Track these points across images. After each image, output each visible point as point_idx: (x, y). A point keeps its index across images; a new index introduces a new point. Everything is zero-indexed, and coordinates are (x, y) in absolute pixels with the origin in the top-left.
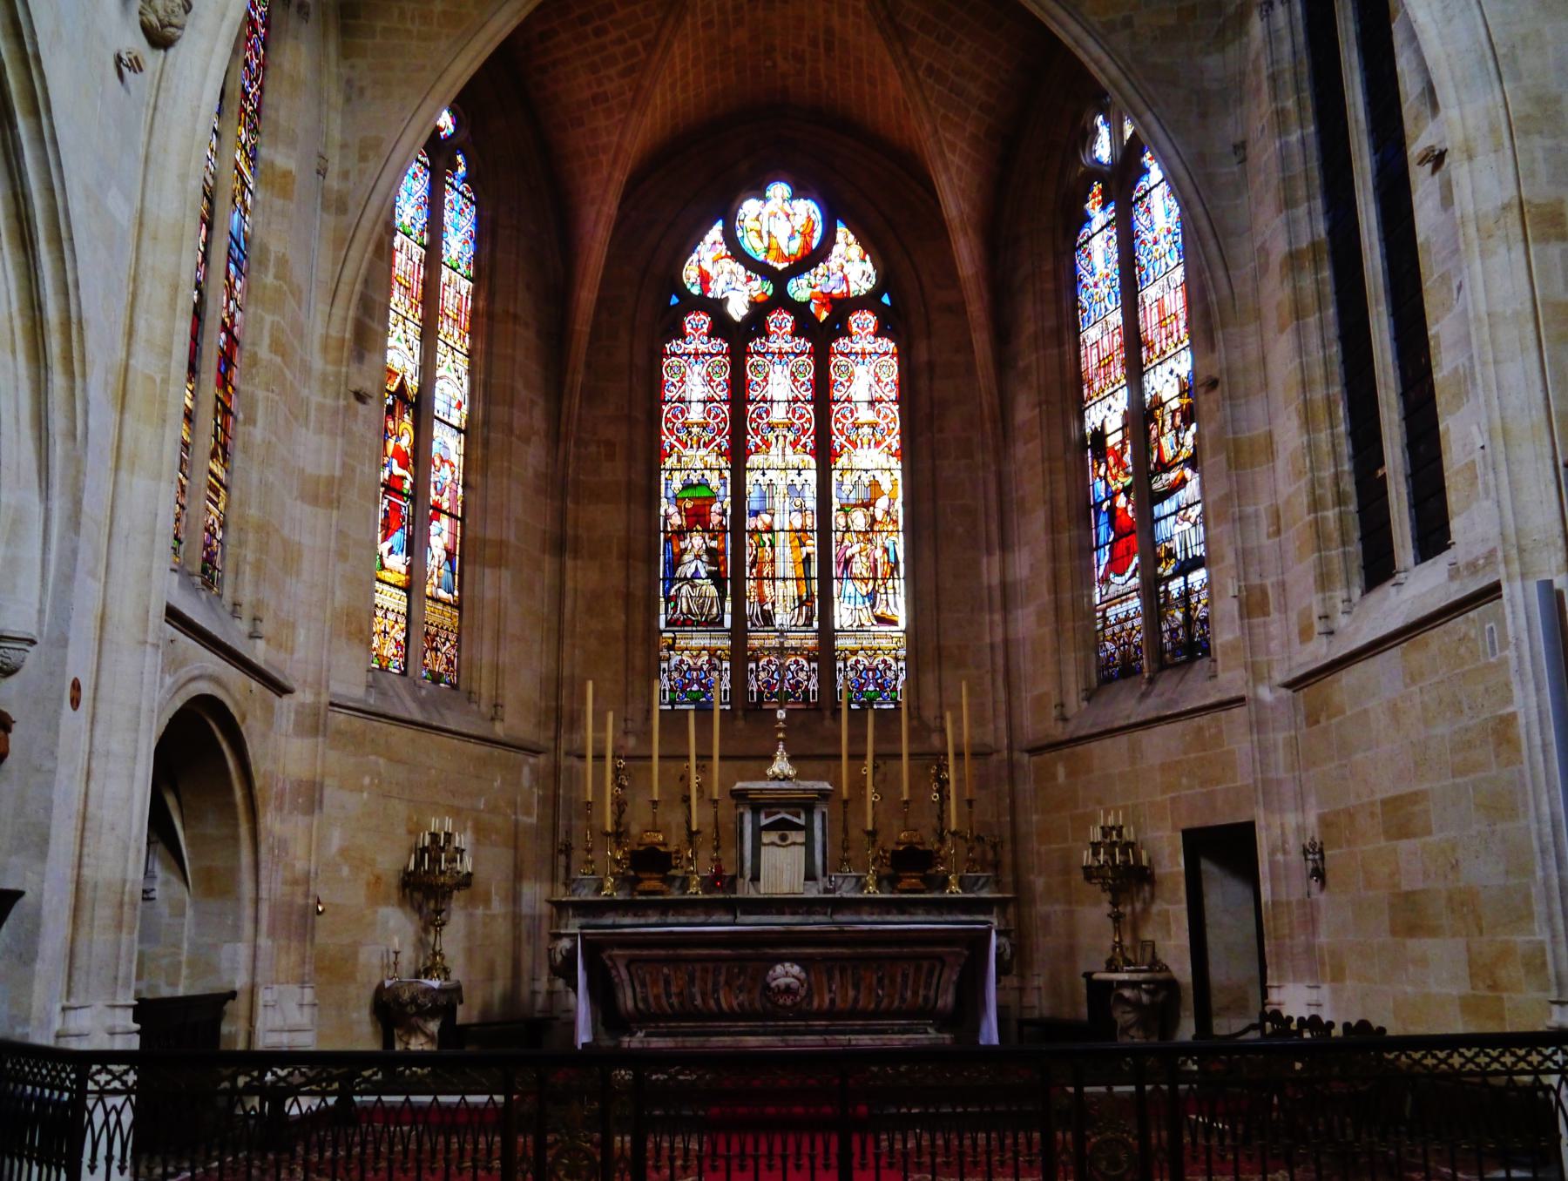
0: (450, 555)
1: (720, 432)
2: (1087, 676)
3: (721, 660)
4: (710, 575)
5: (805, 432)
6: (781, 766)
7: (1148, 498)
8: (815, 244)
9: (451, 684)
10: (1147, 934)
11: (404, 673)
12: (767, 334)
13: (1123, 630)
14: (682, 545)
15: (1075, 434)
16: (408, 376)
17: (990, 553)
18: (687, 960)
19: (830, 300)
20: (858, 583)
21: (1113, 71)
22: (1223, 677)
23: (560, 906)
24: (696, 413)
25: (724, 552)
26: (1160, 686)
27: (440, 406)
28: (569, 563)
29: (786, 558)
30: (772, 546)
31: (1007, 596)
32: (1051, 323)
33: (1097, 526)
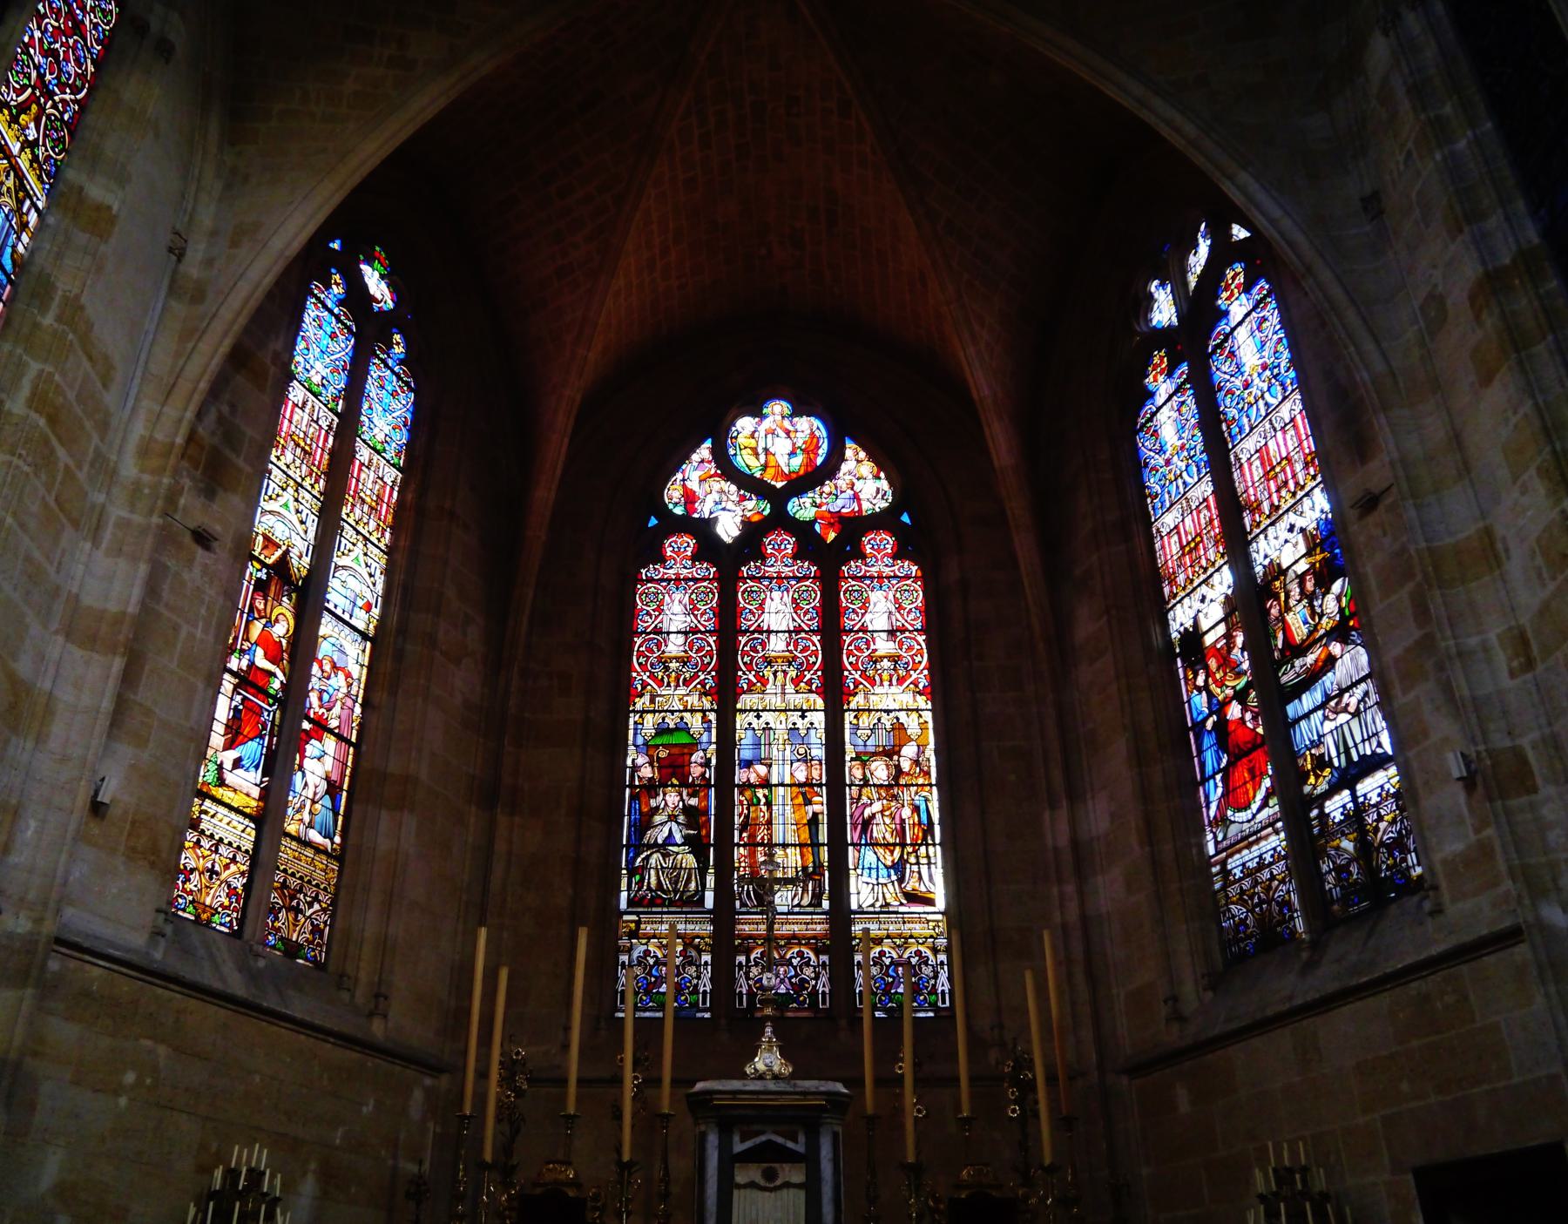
0: (333, 789)
1: (704, 668)
3: (700, 952)
5: (810, 667)
6: (768, 1060)
7: (1273, 697)
8: (819, 461)
9: (314, 960)
11: (236, 935)
12: (763, 557)
13: (1256, 883)
14: (653, 803)
15: (1157, 640)
16: (294, 553)
17: (1053, 806)
20: (880, 851)
21: (1190, 129)
22: (1454, 910)
24: (675, 646)
25: (706, 812)
27: (336, 597)
28: (503, 820)
29: (785, 820)
30: (769, 804)
31: (1082, 860)
33: (1200, 751)
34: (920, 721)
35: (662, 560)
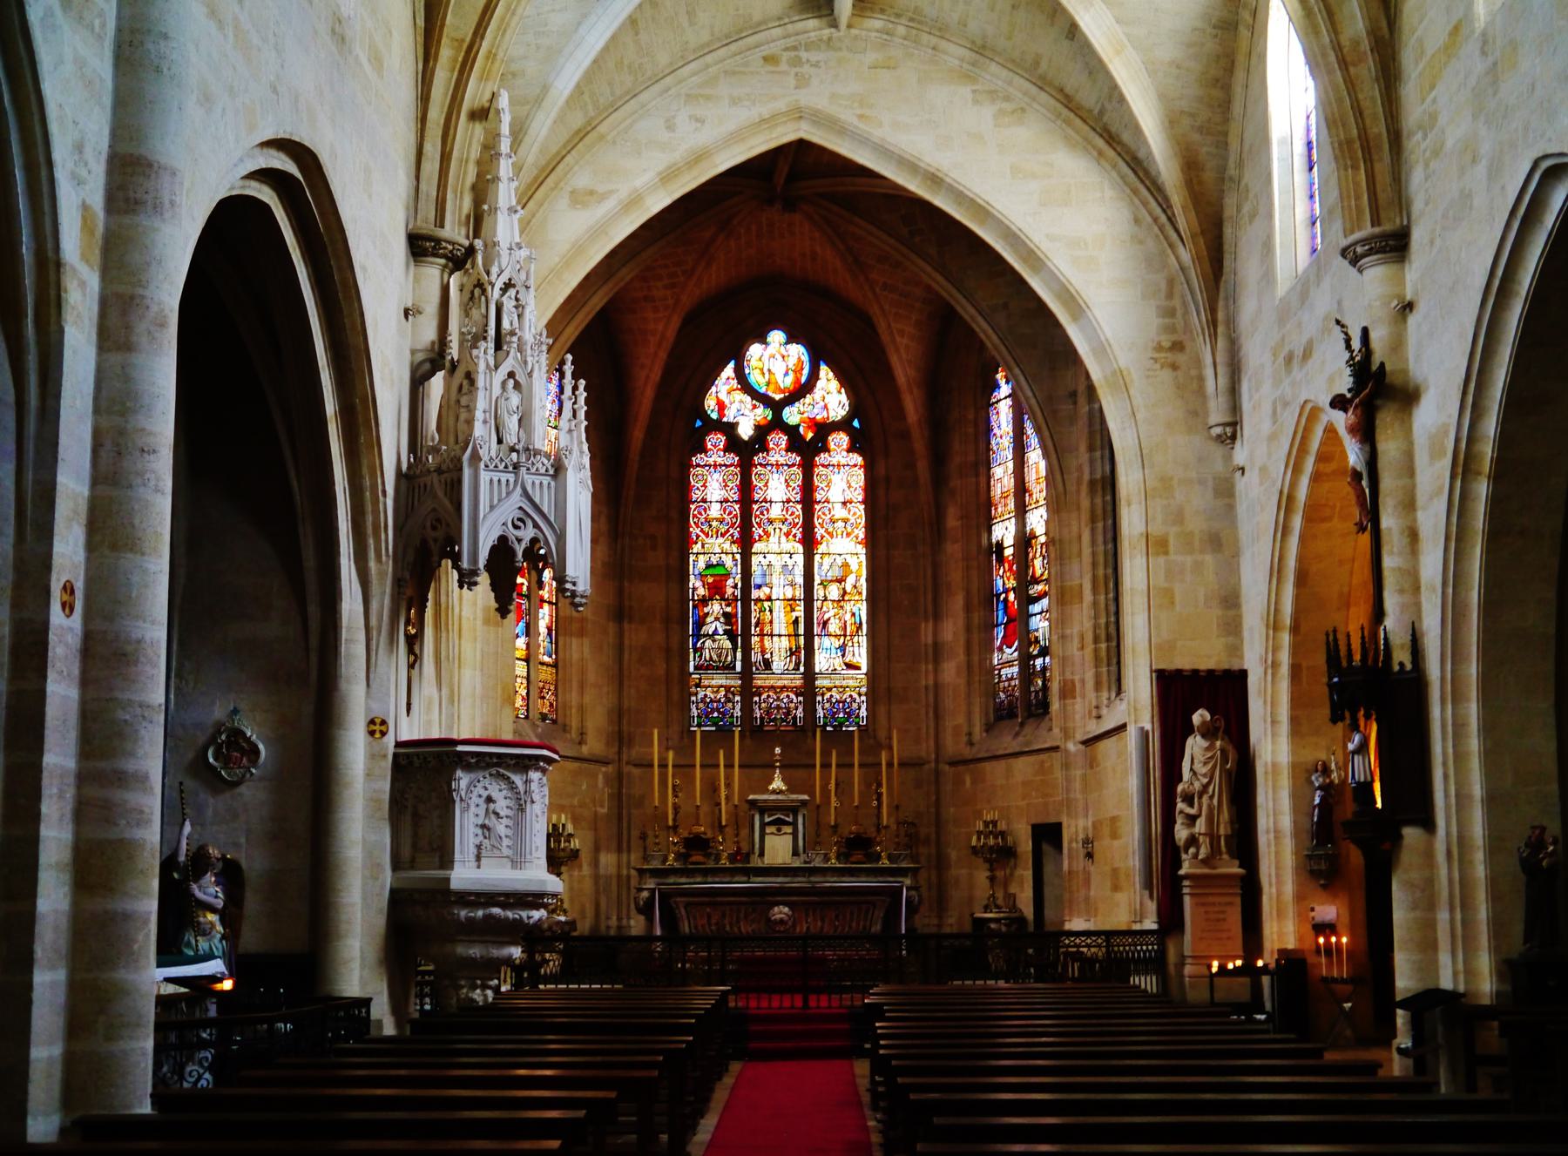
0: (549, 629)
2: (987, 714)
4: (726, 632)
5: (795, 525)
6: (778, 784)
8: (803, 379)
10: (1012, 890)
11: (527, 717)
15: (985, 541)
17: (927, 620)
18: (722, 904)
19: (815, 424)
23: (641, 872)
24: (715, 511)
25: (736, 615)
26: (1028, 729)
28: (626, 626)
29: (780, 620)
31: (937, 652)
32: (971, 458)
34: (858, 559)
35: (704, 450)
